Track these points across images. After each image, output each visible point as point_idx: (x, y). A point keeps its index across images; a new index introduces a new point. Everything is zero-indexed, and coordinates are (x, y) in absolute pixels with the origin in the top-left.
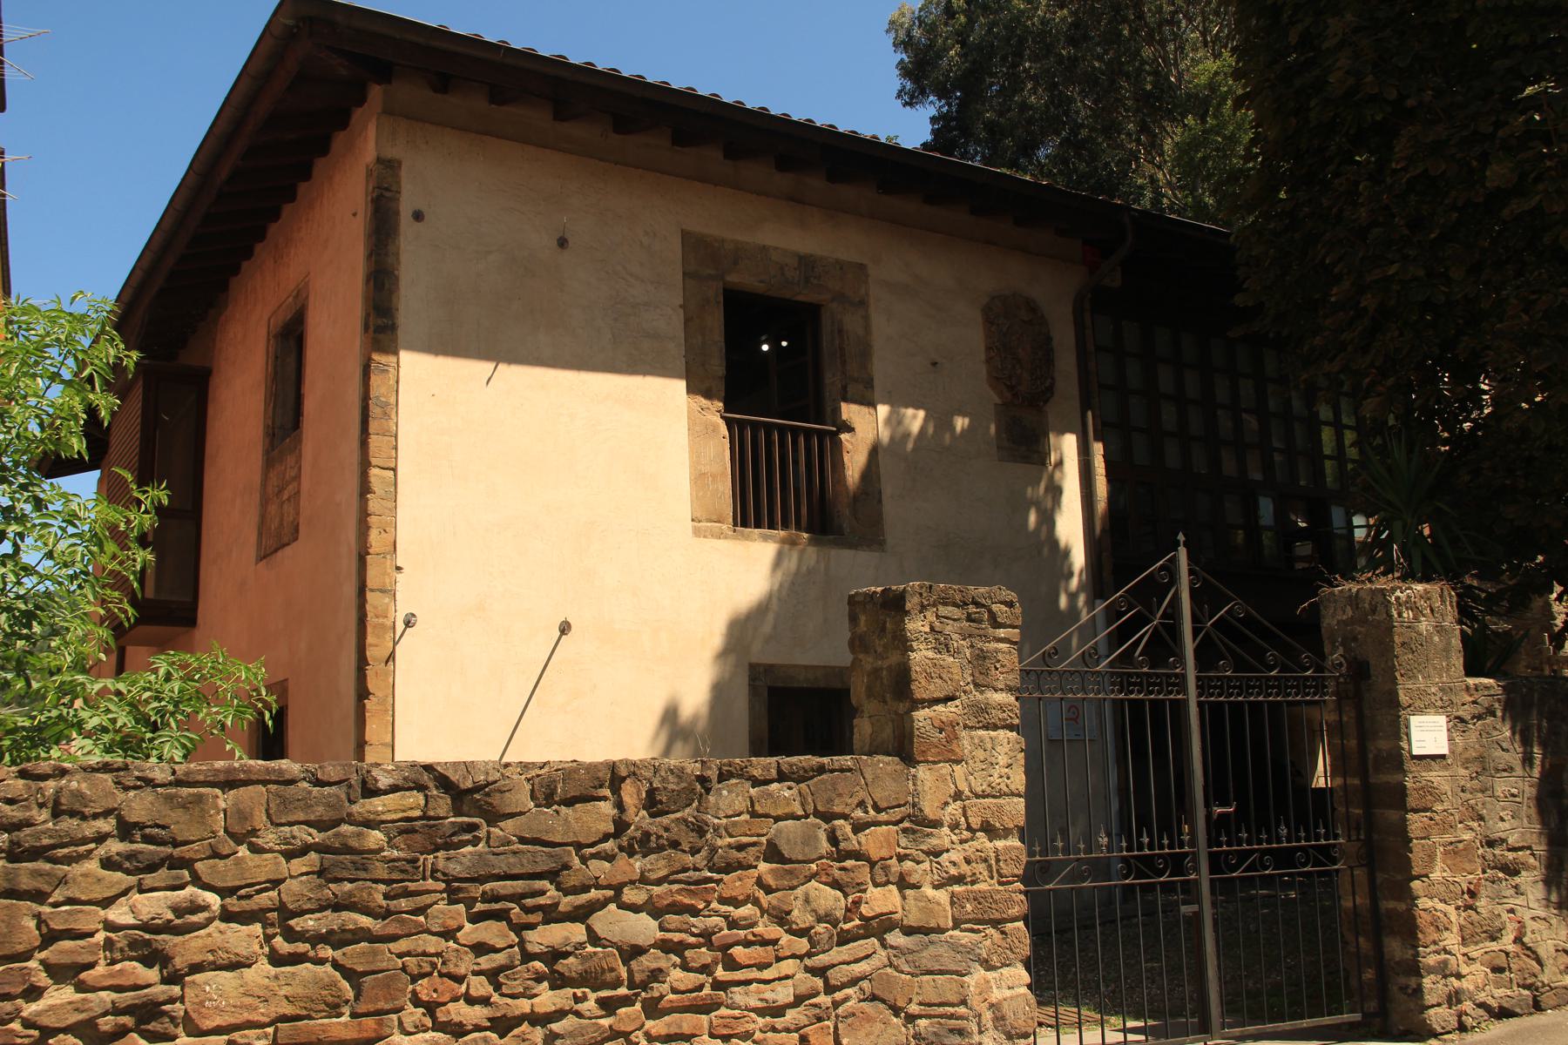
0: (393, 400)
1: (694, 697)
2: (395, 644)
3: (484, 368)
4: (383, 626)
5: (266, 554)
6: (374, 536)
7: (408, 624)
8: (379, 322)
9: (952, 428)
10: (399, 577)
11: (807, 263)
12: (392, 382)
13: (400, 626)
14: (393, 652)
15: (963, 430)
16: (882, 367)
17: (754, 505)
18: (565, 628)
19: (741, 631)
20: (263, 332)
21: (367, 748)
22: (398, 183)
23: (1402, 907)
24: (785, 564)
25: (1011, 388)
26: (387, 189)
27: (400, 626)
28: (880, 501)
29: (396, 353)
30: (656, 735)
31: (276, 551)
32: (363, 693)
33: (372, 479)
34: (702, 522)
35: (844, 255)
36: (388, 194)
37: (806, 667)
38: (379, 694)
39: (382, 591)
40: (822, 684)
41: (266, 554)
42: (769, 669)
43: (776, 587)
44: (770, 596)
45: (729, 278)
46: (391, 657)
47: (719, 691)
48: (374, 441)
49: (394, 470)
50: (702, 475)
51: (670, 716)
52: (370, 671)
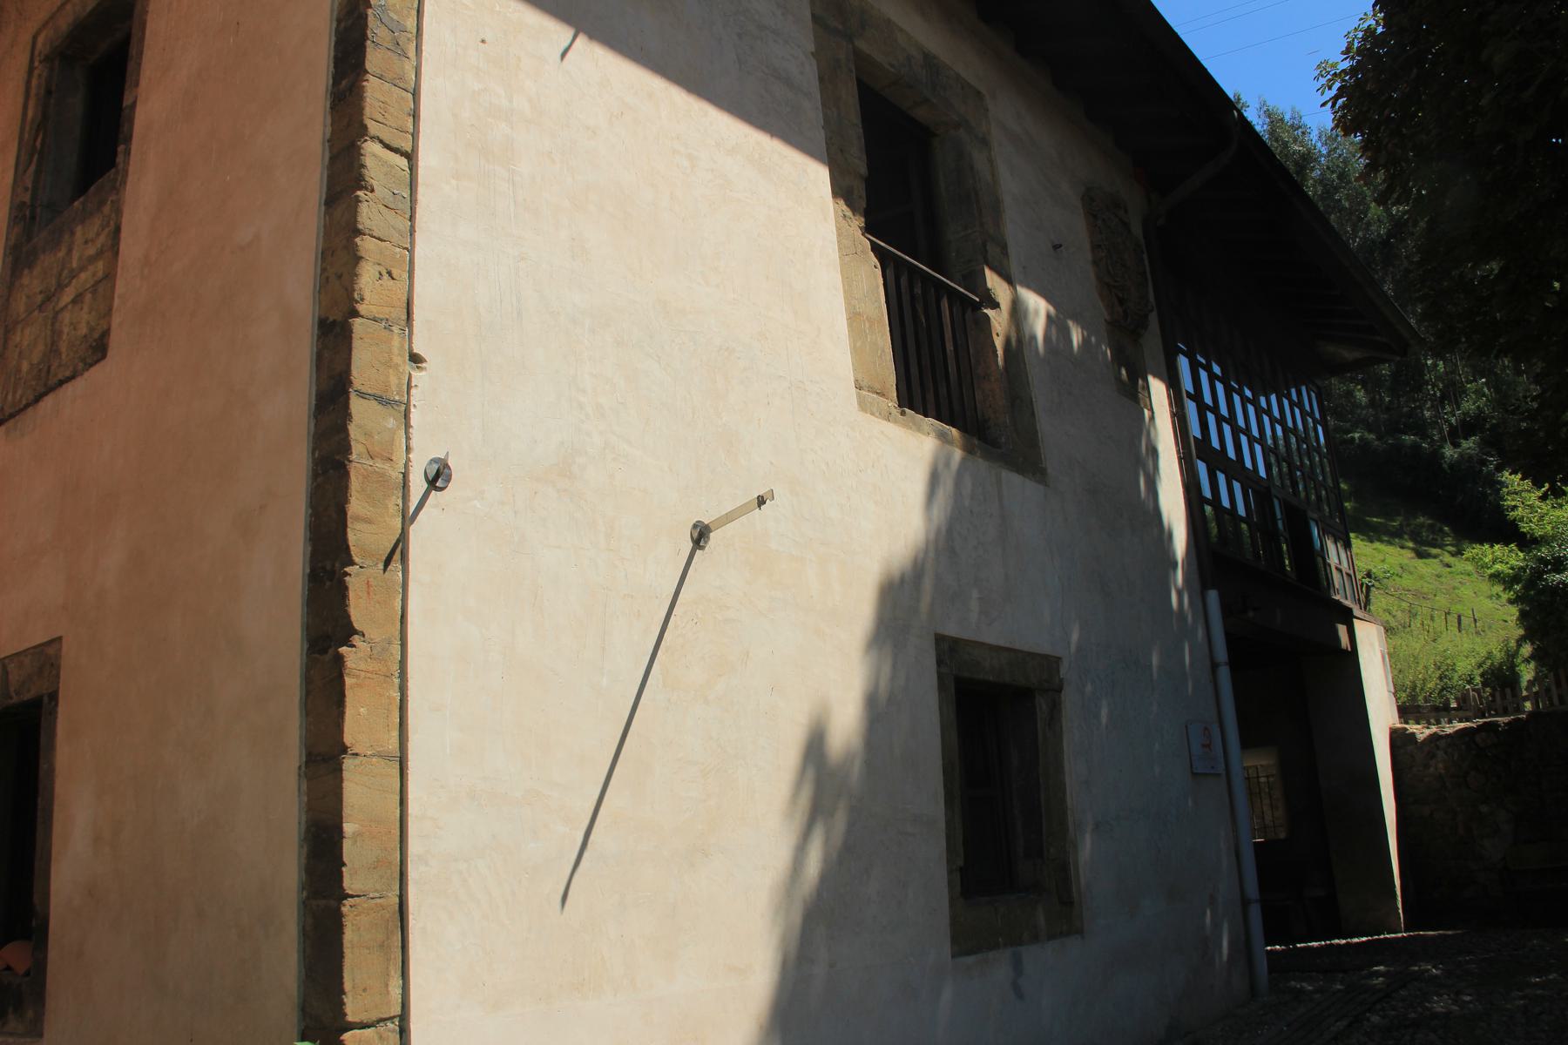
0: (411, 24)
2: (408, 519)
3: (560, 33)
4: (382, 478)
6: (367, 278)
7: (438, 477)
10: (417, 376)
13: (418, 485)
14: (403, 539)
16: (1014, 229)
18: (701, 535)
19: (899, 602)
20: (23, 60)
21: (348, 764)
23: (333, 903)
25: (1121, 301)
27: (418, 485)
32: (328, 629)
33: (368, 161)
38: (371, 633)
39: (380, 400)
46: (398, 552)
47: (877, 710)
48: (374, 90)
49: (411, 157)
51: (815, 748)
52: (356, 580)
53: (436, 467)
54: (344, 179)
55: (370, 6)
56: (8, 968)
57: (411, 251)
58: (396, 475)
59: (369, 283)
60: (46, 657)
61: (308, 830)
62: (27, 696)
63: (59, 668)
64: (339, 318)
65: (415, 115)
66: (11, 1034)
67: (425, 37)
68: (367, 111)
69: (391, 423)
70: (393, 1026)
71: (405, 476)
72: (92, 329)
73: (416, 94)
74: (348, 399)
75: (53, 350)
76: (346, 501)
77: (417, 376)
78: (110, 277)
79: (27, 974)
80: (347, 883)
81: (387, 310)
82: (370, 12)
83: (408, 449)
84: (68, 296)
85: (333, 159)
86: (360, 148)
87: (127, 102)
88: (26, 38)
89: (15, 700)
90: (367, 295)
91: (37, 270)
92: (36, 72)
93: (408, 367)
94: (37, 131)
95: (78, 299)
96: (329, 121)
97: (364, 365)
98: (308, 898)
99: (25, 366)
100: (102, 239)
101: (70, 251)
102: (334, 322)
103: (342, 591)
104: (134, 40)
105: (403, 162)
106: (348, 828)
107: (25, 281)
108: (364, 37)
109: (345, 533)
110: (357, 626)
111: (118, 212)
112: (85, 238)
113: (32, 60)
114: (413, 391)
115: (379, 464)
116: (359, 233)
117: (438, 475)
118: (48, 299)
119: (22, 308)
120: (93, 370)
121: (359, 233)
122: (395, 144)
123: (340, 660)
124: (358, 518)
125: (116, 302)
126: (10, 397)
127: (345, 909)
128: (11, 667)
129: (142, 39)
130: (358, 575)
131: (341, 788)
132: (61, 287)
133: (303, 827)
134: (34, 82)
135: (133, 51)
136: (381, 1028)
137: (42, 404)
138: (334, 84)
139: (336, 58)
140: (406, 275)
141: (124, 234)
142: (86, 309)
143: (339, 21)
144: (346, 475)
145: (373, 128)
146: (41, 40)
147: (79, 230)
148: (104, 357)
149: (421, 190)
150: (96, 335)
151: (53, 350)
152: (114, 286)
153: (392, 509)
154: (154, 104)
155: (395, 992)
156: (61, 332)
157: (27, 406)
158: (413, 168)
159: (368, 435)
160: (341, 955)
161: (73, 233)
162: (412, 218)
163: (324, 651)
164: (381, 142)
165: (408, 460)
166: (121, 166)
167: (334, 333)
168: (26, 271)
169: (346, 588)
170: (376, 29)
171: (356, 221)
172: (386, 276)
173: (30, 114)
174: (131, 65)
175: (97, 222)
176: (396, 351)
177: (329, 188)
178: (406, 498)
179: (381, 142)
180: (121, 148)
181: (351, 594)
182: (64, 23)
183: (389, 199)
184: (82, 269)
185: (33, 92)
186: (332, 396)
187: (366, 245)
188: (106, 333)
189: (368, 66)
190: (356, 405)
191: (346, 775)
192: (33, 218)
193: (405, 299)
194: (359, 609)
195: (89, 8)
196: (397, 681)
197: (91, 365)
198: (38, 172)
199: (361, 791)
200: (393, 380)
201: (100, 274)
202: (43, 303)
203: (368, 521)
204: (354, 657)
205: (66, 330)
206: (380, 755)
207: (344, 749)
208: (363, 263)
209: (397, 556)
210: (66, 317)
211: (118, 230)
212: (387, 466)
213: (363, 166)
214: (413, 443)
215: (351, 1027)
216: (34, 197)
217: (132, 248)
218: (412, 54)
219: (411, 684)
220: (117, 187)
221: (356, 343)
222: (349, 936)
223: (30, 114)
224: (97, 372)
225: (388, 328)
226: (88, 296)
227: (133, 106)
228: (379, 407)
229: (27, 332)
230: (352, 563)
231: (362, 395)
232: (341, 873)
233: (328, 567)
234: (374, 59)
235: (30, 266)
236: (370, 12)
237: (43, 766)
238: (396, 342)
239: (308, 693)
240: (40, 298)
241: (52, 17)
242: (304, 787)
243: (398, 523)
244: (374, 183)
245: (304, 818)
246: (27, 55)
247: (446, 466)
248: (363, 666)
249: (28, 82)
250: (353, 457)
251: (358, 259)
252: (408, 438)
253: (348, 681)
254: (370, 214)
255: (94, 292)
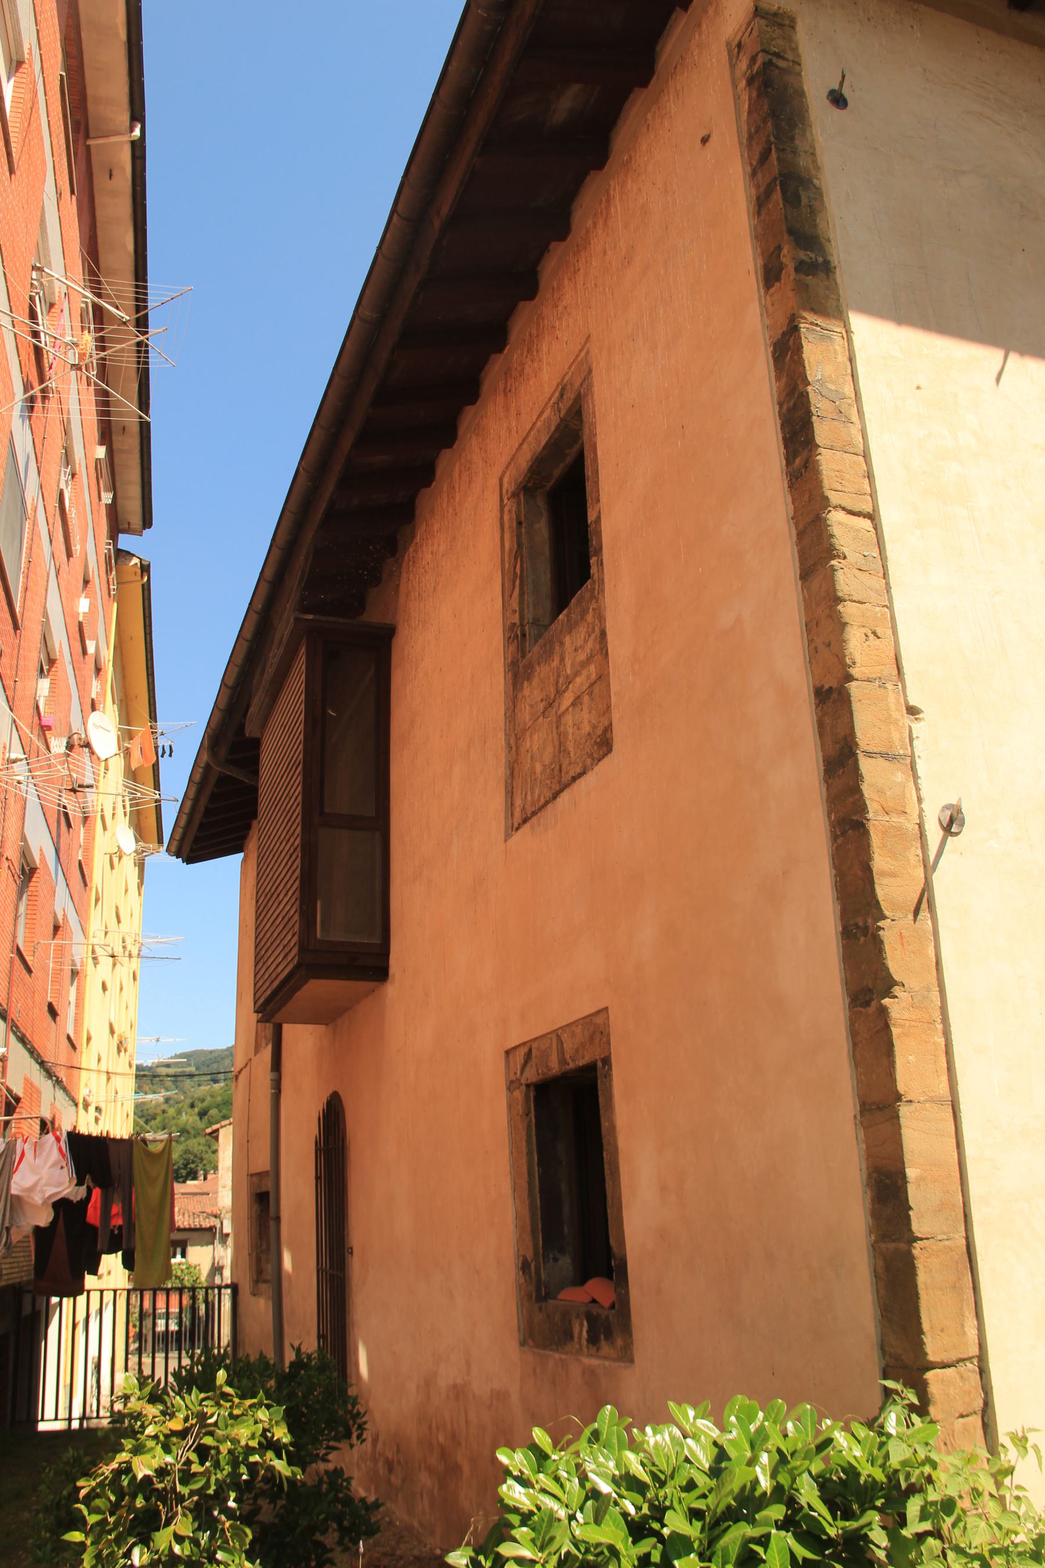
0: (848, 390)
2: (929, 869)
3: (990, 357)
5: (521, 817)
6: (856, 644)
7: (952, 823)
8: (802, 255)
10: (918, 728)
12: (842, 358)
13: (934, 834)
20: (493, 501)
21: (904, 1110)
22: (795, 50)
23: (902, 1246)
26: (777, 55)
27: (934, 834)
29: (840, 315)
31: (555, 796)
32: (868, 984)
33: (836, 530)
34: (528, 1052)
36: (781, 64)
39: (885, 756)
41: (521, 817)
46: (924, 901)
48: (828, 462)
49: (872, 516)
52: (889, 934)
53: (948, 813)
54: (815, 553)
55: (809, 384)
56: (594, 1301)
57: (890, 607)
58: (912, 827)
59: (860, 649)
60: (596, 1026)
61: (869, 1176)
62: (581, 1063)
63: (609, 1034)
64: (834, 684)
65: (870, 476)
66: (606, 1358)
67: (864, 398)
68: (826, 483)
69: (899, 777)
70: (972, 1367)
71: (921, 826)
72: (594, 727)
73: (866, 456)
74: (856, 761)
75: (561, 749)
76: (870, 858)
77: (918, 728)
78: (603, 677)
79: (612, 1307)
80: (914, 1226)
81: (878, 668)
82: (809, 389)
83: (920, 800)
84: (568, 699)
85: (801, 535)
86: (825, 520)
87: (591, 517)
88: (494, 482)
89: (572, 1066)
90: (858, 658)
91: (535, 681)
92: (506, 509)
93: (907, 720)
94: (516, 559)
95: (576, 702)
96: (789, 499)
97: (868, 725)
98: (876, 1242)
99: (538, 768)
100: (590, 645)
101: (562, 659)
102: (831, 688)
103: (878, 944)
104: (588, 462)
105: (867, 524)
106: (911, 1173)
107: (526, 691)
108: (809, 414)
109: (873, 890)
110: (896, 977)
111: (601, 618)
112: (574, 645)
113: (501, 500)
114: (915, 743)
115: (895, 819)
116: (839, 600)
117: (951, 821)
118: (550, 705)
119: (527, 717)
120: (601, 764)
121: (839, 600)
122: (856, 509)
123: (883, 1011)
124: (883, 874)
125: (613, 699)
126: (529, 797)
127: (916, 1252)
128: (565, 1037)
129: (595, 460)
130: (890, 928)
131: (900, 1135)
132: (559, 693)
133: (865, 1177)
134: (506, 517)
135: (589, 472)
136: (961, 1367)
137: (559, 800)
138: (788, 464)
139: (784, 439)
140: (890, 632)
141: (610, 638)
142: (585, 708)
143: (781, 405)
144: (866, 833)
145: (834, 498)
146: (506, 480)
147: (567, 640)
148: (610, 750)
149: (889, 546)
150: (599, 732)
151: (561, 749)
152: (609, 685)
153: (913, 860)
154: (616, 513)
155: (972, 1333)
156: (566, 734)
157: (547, 803)
158: (877, 528)
159: (881, 792)
160: (917, 1296)
161: (562, 644)
162: (885, 576)
163: (867, 1004)
164: (844, 509)
165: (921, 810)
166: (596, 577)
167: (832, 699)
168: (526, 684)
169: (882, 942)
170: (818, 404)
171: (835, 590)
172: (871, 637)
173: (507, 545)
174: (589, 486)
175: (582, 630)
176: (893, 707)
177: (801, 564)
178: (924, 847)
179: (844, 509)
180: (593, 560)
181: (887, 947)
182: (524, 462)
183: (861, 562)
184: (577, 674)
185: (506, 526)
186: (842, 761)
187: (848, 610)
188: (608, 729)
189: (819, 440)
190: (865, 765)
191: (902, 1121)
192: (524, 635)
193: (892, 655)
194: (897, 961)
195: (543, 443)
196: (940, 1027)
197: (599, 761)
198: (522, 594)
199: (920, 1138)
200: (895, 736)
201: (594, 677)
202: (546, 709)
203: (893, 875)
204: (897, 1007)
205: (570, 731)
206: (932, 1100)
207: (899, 1097)
208: (848, 629)
209: (924, 905)
210: (569, 719)
211: (603, 634)
212: (902, 820)
213: (832, 536)
214: (923, 793)
215: (931, 1366)
216: (522, 617)
217: (619, 648)
218: (855, 418)
219: (954, 1029)
220: (596, 596)
221: (856, 706)
222: (922, 1278)
223: (507, 545)
224: (606, 765)
225: (882, 686)
226: (586, 698)
227: (598, 519)
228: (887, 763)
229: (536, 737)
230: (884, 918)
231: (869, 754)
232: (909, 1216)
233: (860, 924)
234: (822, 432)
235: (529, 678)
236: (809, 389)
237: (605, 1124)
238: (891, 698)
239: (855, 1045)
240: (541, 706)
241: (512, 459)
242: (861, 1135)
243: (920, 873)
244: (845, 550)
245: (864, 1166)
246: (497, 496)
247: (959, 811)
248: (906, 1015)
249: (502, 518)
250: (870, 815)
251: (843, 625)
252: (918, 789)
253: (895, 1031)
254: (846, 581)
255: (591, 694)
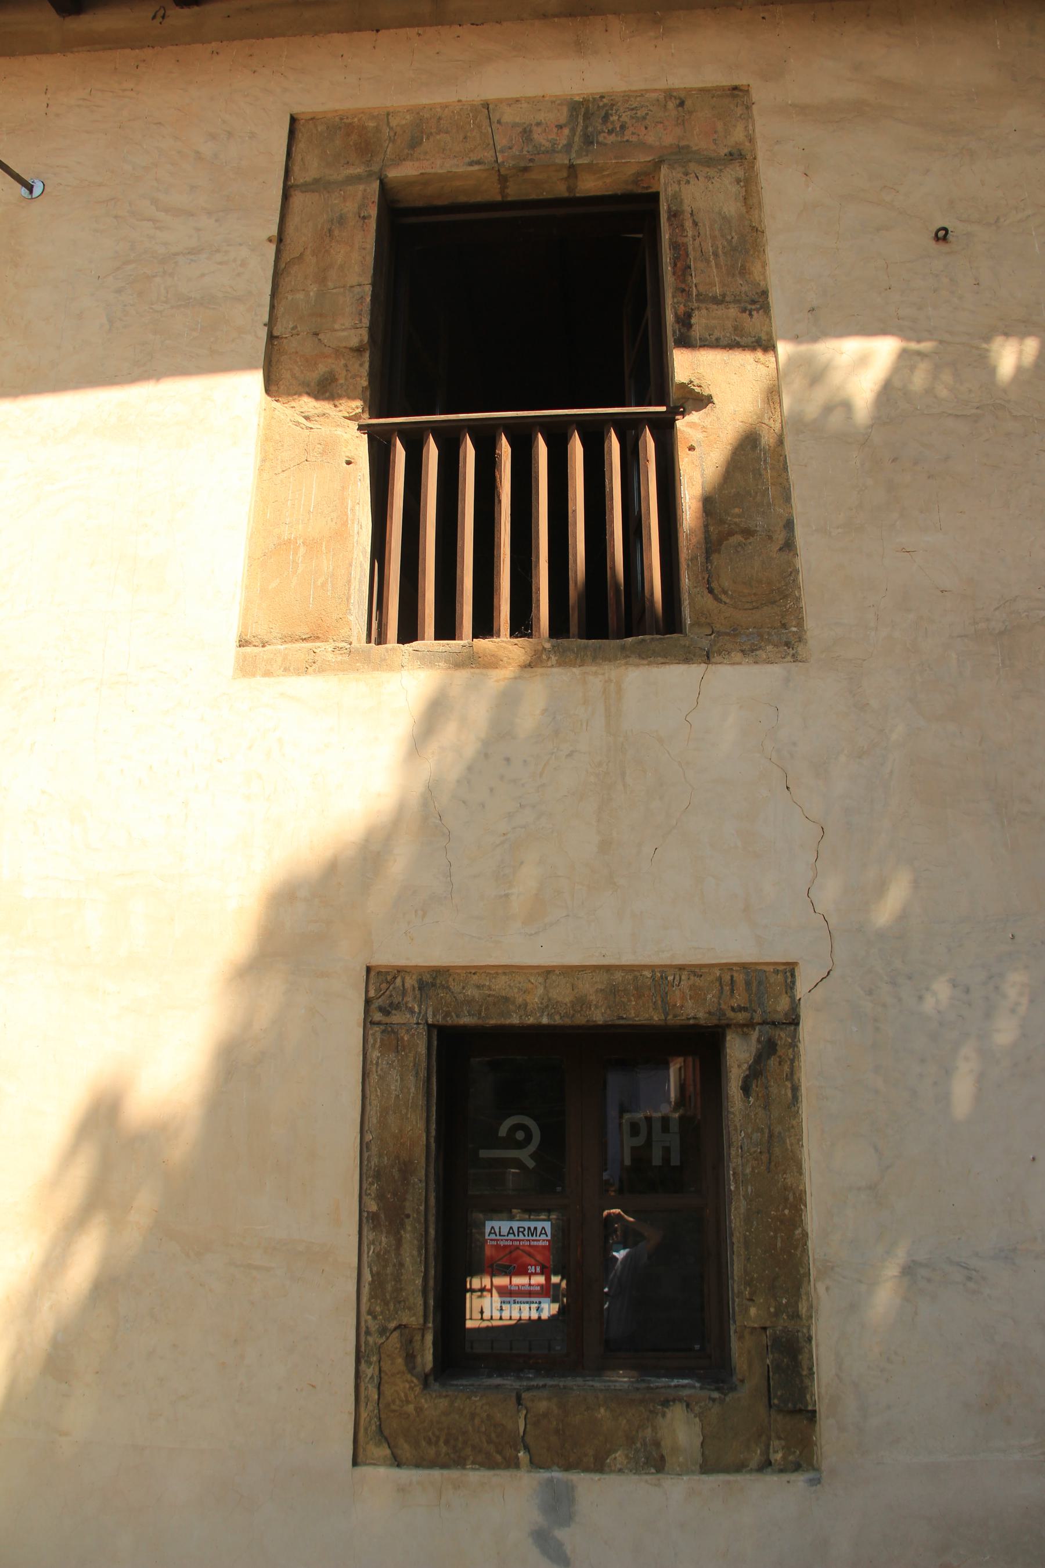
1: (169, 1066)
9: (986, 365)
11: (589, 115)
15: (1019, 369)
17: (423, 590)
24: (449, 733)
28: (789, 545)
30: (56, 1181)
35: (714, 77)
37: (547, 972)
40: (599, 1016)
42: (433, 981)
43: (418, 788)
44: (401, 808)
45: (393, 173)
47: (236, 1067)
50: (286, 545)
51: (103, 1123)
